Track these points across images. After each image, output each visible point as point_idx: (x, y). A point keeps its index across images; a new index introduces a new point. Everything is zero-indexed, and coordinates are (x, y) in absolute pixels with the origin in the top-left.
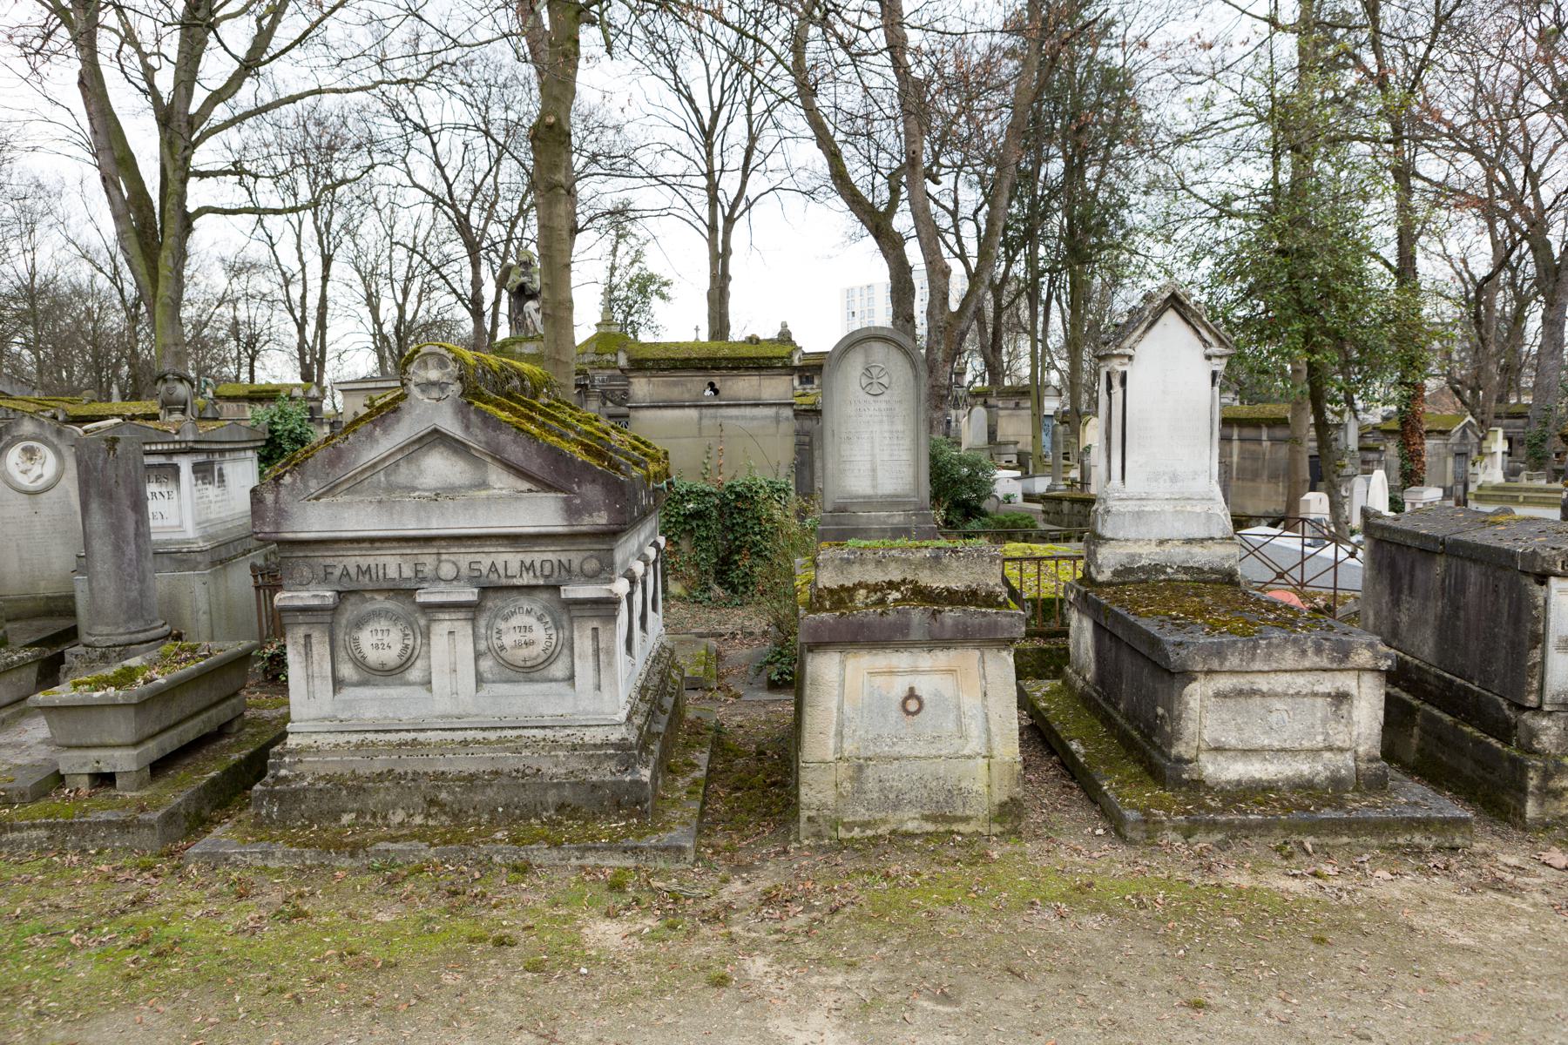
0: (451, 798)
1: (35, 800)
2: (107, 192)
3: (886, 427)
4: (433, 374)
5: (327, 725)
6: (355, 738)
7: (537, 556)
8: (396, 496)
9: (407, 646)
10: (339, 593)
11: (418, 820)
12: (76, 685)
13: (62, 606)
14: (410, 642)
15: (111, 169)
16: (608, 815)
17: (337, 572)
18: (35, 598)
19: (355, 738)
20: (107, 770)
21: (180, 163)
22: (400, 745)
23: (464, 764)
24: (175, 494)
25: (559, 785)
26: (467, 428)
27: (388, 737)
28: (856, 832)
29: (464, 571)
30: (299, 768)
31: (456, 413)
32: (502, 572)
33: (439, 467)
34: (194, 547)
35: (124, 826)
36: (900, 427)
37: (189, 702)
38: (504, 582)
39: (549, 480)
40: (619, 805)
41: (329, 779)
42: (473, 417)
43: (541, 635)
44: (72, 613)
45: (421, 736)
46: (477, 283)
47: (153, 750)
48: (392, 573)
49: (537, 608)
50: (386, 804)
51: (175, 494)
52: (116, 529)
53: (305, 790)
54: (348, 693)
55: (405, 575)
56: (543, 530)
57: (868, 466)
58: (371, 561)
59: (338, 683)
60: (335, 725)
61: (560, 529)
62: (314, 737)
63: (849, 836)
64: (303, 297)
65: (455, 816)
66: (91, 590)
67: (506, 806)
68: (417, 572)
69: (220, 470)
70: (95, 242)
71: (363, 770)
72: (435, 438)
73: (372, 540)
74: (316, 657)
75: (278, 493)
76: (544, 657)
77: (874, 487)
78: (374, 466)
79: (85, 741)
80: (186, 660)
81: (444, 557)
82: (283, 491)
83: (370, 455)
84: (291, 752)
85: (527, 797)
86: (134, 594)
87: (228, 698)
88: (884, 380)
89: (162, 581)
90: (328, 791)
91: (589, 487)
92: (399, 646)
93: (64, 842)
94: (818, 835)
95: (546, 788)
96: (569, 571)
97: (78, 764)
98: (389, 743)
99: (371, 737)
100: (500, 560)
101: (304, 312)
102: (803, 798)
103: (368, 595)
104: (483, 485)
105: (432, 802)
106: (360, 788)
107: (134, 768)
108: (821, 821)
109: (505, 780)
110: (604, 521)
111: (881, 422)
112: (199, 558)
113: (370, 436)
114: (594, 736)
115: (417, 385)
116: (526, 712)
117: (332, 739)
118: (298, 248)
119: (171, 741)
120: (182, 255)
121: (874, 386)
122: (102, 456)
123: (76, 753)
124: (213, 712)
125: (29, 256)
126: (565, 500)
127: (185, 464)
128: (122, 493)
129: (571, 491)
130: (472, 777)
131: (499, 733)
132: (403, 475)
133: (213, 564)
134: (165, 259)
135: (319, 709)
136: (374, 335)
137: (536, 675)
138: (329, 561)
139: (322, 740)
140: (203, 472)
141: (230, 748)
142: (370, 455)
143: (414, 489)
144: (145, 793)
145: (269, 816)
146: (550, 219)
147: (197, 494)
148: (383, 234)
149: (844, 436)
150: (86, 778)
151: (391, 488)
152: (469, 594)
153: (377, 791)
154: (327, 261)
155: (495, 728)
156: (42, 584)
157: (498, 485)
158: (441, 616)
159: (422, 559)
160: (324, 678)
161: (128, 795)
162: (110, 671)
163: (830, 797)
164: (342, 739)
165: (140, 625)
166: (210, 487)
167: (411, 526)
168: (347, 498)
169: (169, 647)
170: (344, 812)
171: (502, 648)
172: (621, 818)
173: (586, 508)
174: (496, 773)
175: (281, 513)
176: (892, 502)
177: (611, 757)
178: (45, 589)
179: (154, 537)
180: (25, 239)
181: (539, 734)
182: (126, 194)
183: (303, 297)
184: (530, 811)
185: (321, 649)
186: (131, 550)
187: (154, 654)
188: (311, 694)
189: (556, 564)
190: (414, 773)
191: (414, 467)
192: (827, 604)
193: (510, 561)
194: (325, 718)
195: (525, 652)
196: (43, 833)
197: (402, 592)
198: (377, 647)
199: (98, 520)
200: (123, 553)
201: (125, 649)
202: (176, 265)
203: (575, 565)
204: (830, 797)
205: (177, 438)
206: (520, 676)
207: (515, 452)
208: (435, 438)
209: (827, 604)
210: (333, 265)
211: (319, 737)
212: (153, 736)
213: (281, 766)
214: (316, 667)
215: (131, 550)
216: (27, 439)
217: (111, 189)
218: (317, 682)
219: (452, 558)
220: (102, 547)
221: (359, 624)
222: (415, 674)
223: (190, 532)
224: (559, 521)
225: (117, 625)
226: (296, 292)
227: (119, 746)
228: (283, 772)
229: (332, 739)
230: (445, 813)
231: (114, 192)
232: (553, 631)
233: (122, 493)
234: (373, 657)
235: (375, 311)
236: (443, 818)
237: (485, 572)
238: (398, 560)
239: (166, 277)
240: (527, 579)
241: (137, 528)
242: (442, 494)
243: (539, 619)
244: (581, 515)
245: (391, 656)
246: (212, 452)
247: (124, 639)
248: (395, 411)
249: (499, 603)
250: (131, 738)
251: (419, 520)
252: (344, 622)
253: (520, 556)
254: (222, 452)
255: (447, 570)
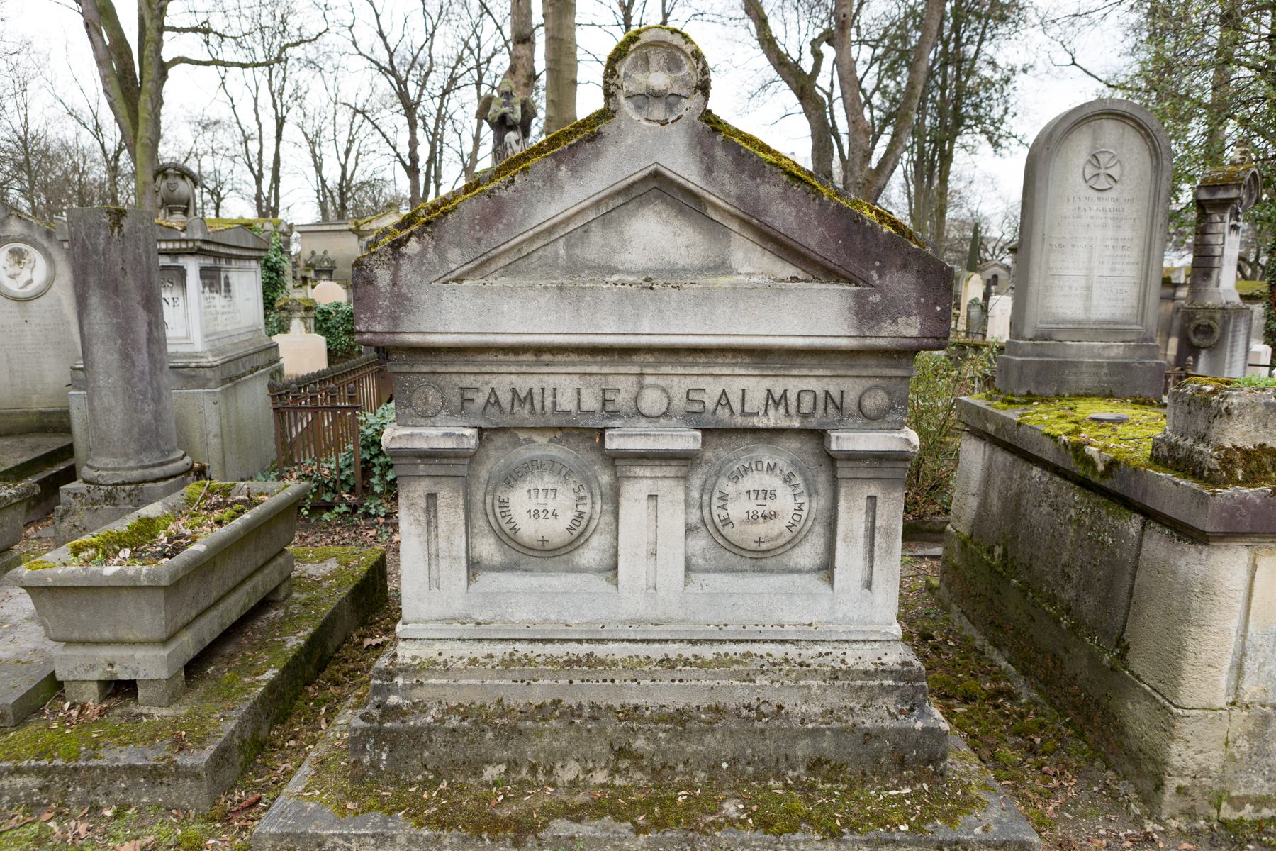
0: (651, 747)
1: (20, 722)
2: (90, 38)
3: (1110, 233)
4: (659, 80)
5: (457, 630)
6: (499, 650)
7: (792, 384)
8: (583, 279)
9: (581, 515)
10: (481, 430)
11: (600, 777)
12: (76, 551)
13: (58, 423)
14: (586, 509)
15: (93, 15)
16: (885, 777)
17: (481, 399)
18: (27, 413)
19: (499, 650)
20: (126, 677)
21: (157, 12)
22: (569, 663)
23: (666, 695)
24: (180, 301)
25: (815, 733)
26: (709, 170)
27: (549, 649)
28: (1248, 812)
29: (679, 403)
30: (418, 695)
31: (692, 146)
32: (736, 406)
33: (654, 236)
34: (204, 362)
35: (155, 775)
36: (1127, 233)
37: (231, 571)
38: (739, 421)
39: (834, 260)
40: (902, 763)
41: (465, 712)
42: (719, 153)
43: (787, 503)
44: (67, 429)
45: (600, 651)
46: (413, 143)
47: (188, 644)
48: (566, 402)
49: (783, 463)
50: (552, 753)
51: (180, 301)
52: (124, 330)
53: (429, 729)
54: (487, 581)
55: (585, 407)
56: (817, 342)
57: (1083, 282)
58: (534, 383)
59: (474, 566)
60: (469, 630)
61: (844, 343)
62: (438, 646)
63: (1235, 816)
64: (260, 153)
65: (655, 773)
66: (92, 410)
67: (734, 761)
68: (604, 402)
69: (226, 278)
70: (80, 104)
71: (517, 698)
72: (657, 187)
73: (539, 350)
74: (442, 527)
75: (397, 269)
76: (788, 536)
77: (1087, 309)
78: (551, 230)
79: (92, 635)
80: (218, 506)
81: (648, 380)
82: (405, 266)
83: (549, 210)
84: (405, 670)
85: (766, 748)
86: (147, 417)
87: (274, 558)
88: (1114, 172)
89: (178, 396)
90: (465, 732)
91: (897, 275)
92: (570, 515)
93: (64, 795)
94: (1190, 814)
95: (796, 736)
96: (840, 408)
97: (82, 668)
98: (552, 660)
99: (523, 648)
100: (734, 387)
101: (260, 165)
102: (1175, 761)
103: (522, 436)
104: (721, 267)
105: (622, 753)
106: (514, 729)
107: (164, 674)
108: (1197, 793)
109: (733, 723)
110: (914, 332)
111: (1105, 226)
112: (209, 374)
113: (550, 179)
114: (862, 657)
115: (629, 97)
116: (757, 617)
117: (466, 650)
118: (256, 110)
119: (210, 627)
120: (158, 102)
121: (1100, 176)
122: (103, 233)
123: (79, 651)
124: (258, 578)
125: (22, 112)
126: (856, 296)
127: (192, 267)
128: (130, 283)
129: (867, 282)
130: (681, 718)
131: (716, 648)
132: (595, 248)
133: (223, 381)
134: (144, 101)
135: (453, 602)
136: (318, 191)
137: (770, 563)
138: (468, 381)
139: (449, 650)
140: (211, 277)
141: (281, 625)
142: (549, 210)
143: (612, 270)
144: (182, 711)
145: (374, 765)
146: (559, 29)
147: (204, 303)
148: (326, 100)
149: (1055, 242)
150: (95, 687)
151: (574, 268)
152: (688, 440)
153: (540, 734)
154: (280, 122)
155: (711, 641)
156: (35, 398)
157: (746, 269)
158: (639, 471)
159: (613, 382)
160: (454, 559)
161: (158, 713)
162: (122, 526)
163: (1214, 759)
164: (480, 651)
165: (154, 457)
166: (217, 296)
167: (608, 329)
168: (506, 281)
169: (194, 488)
170: (488, 763)
171: (727, 521)
172: (904, 782)
173: (890, 310)
174: (717, 709)
175: (401, 301)
176: (1109, 330)
177: (887, 691)
178: (39, 403)
179: (170, 349)
180: (19, 98)
181: (778, 651)
182: (108, 43)
183: (260, 153)
184: (768, 768)
185: (450, 515)
186: (142, 360)
187: (176, 498)
188: (434, 583)
189: (821, 396)
190: (593, 706)
191: (613, 236)
192: (1239, 473)
193: (750, 389)
194: (452, 620)
195: (761, 529)
196: (33, 782)
197: (585, 433)
198: (536, 514)
199: (99, 319)
200: (133, 364)
201: (137, 492)
202: (154, 108)
203: (850, 402)
204: (1214, 759)
205: (183, 235)
206: (747, 564)
207: (784, 215)
208: (657, 187)
209: (1239, 473)
210: (285, 127)
211: (446, 647)
212: (187, 625)
213: (390, 691)
214: (443, 543)
215: (142, 360)
216: (14, 240)
217: (94, 34)
218: (443, 564)
219: (661, 381)
220: (105, 355)
221: (510, 478)
222: (590, 555)
223: (199, 345)
224: (845, 329)
225: (126, 456)
226: (254, 146)
227: (142, 643)
228: (393, 700)
229: (466, 650)
230: (641, 769)
231: (97, 38)
232: (803, 499)
233: (130, 283)
234: (529, 529)
235: (318, 168)
236: (638, 775)
237: (710, 405)
238: (577, 382)
239: (146, 120)
240: (774, 419)
241: (150, 332)
242: (653, 281)
243: (787, 479)
244: (878, 322)
245: (556, 529)
246: (218, 256)
247: (136, 474)
248: (594, 138)
249: (724, 454)
250: (160, 633)
251: (622, 319)
252: (484, 475)
253: (767, 383)
254: (229, 258)
255: (652, 401)
